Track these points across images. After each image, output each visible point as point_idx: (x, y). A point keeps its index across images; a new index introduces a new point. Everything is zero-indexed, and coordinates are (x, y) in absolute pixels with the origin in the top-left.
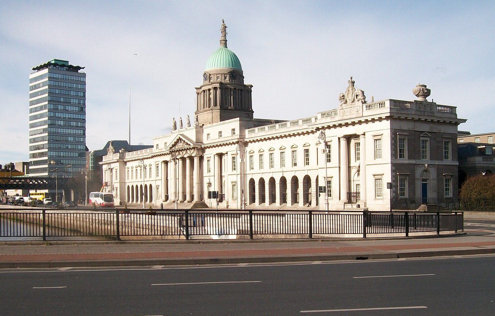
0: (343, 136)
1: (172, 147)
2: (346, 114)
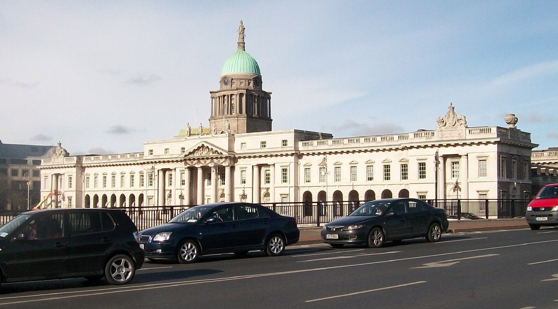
0: (442, 155)
1: (188, 155)
2: (445, 136)
